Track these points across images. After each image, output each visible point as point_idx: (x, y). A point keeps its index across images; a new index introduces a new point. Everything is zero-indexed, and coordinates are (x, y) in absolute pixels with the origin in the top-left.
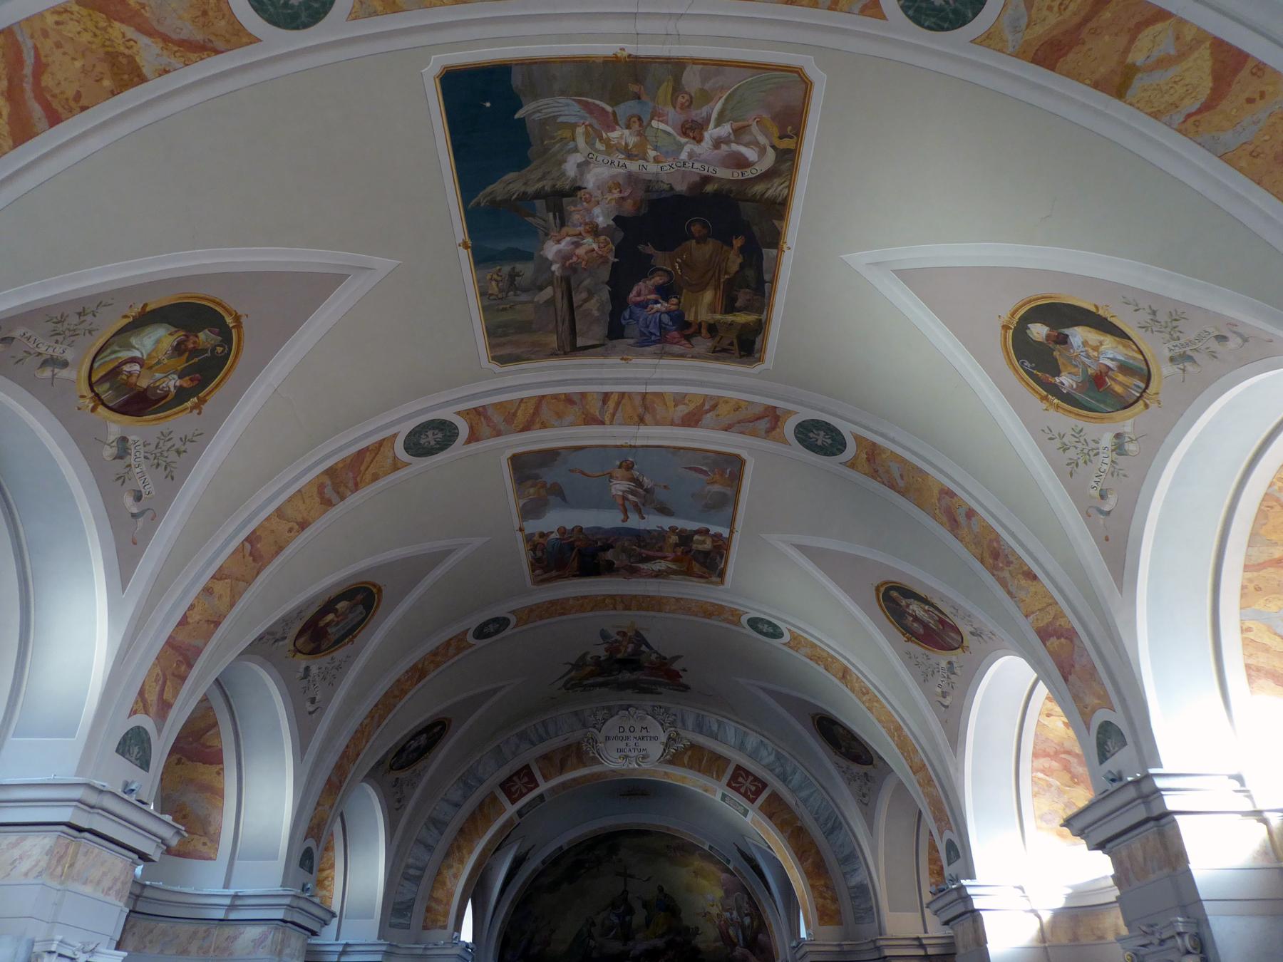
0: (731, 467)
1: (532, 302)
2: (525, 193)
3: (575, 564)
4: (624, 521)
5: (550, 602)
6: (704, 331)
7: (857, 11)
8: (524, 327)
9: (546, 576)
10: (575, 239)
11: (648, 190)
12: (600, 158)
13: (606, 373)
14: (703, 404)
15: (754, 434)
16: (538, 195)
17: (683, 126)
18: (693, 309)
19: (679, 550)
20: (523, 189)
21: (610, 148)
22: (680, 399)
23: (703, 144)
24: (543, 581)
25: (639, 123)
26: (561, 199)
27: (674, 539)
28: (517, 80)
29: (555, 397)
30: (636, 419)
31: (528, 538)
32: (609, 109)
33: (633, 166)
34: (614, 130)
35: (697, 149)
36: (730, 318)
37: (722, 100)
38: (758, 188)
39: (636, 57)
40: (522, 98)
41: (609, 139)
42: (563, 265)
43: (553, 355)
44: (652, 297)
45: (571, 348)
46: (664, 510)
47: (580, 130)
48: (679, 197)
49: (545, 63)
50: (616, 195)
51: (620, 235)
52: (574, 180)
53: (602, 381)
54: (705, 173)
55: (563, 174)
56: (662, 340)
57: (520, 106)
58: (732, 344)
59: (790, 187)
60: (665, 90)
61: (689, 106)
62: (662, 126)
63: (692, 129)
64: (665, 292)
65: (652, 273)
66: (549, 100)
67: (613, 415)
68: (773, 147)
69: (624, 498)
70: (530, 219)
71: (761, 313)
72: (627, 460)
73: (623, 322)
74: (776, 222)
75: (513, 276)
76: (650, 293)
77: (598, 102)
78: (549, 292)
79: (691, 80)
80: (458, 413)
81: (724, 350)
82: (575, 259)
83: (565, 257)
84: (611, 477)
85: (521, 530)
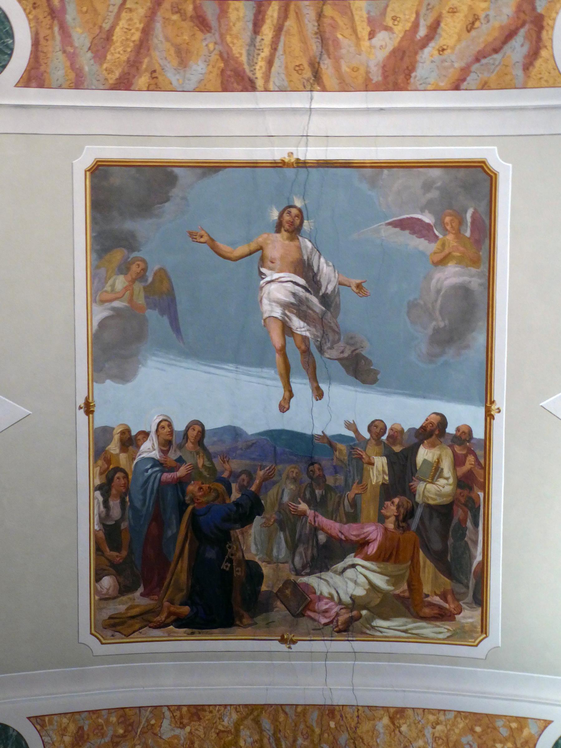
0: (467, 192)
3: (181, 572)
4: (284, 408)
5: (123, 714)
9: (119, 607)
14: (416, 26)
15: (504, 84)
19: (391, 509)
24: (115, 627)
27: (379, 468)
30: (308, 73)
31: (100, 438)
46: (360, 370)
67: (270, 63)
69: (286, 330)
72: (292, 196)
84: (262, 261)
85: (88, 408)
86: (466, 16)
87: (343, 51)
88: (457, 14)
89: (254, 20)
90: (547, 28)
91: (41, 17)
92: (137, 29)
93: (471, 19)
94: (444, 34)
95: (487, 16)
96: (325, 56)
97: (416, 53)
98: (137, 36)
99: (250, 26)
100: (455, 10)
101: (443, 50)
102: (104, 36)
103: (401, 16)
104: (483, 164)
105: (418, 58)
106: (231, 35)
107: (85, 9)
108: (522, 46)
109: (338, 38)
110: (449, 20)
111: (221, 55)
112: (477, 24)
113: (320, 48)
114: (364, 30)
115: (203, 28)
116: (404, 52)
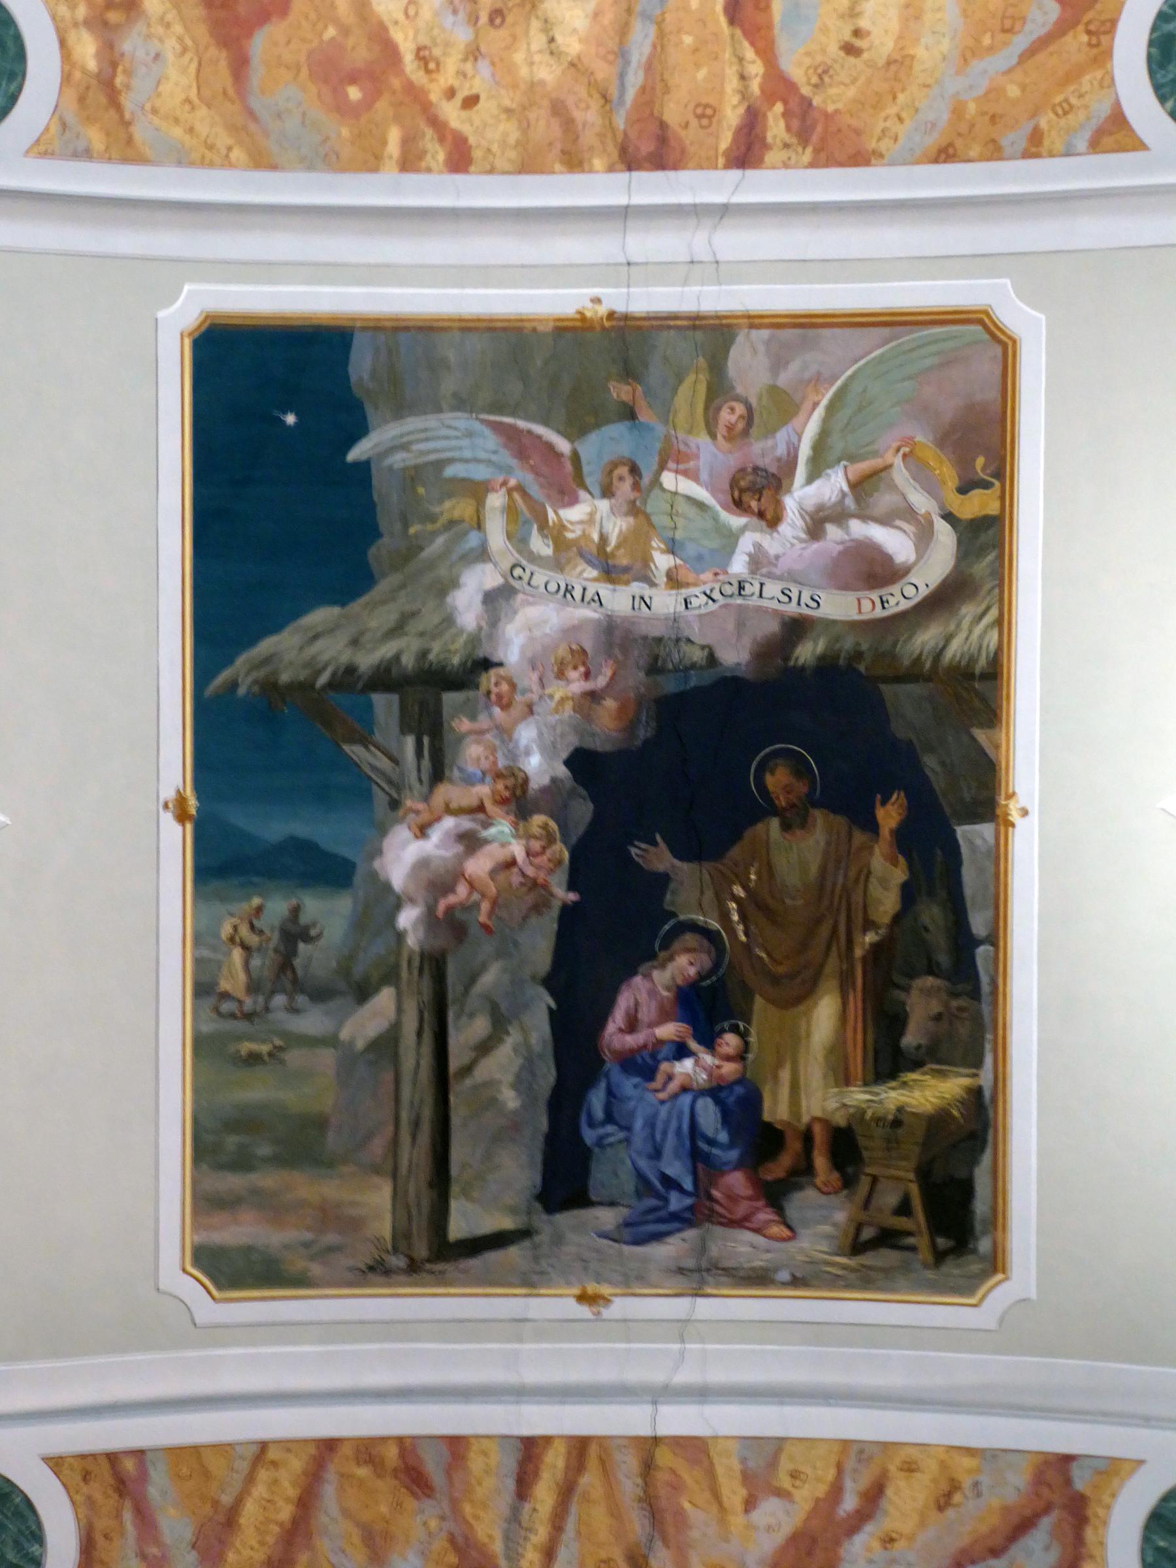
1: (331, 1041)
2: (351, 670)
6: (821, 1161)
7: (1081, 145)
8: (302, 1143)
10: (466, 823)
11: (654, 668)
12: (539, 579)
13: (540, 1364)
14: (836, 1491)
16: (385, 678)
17: (734, 483)
18: (785, 1075)
20: (345, 658)
21: (565, 549)
22: (765, 1464)
23: (783, 528)
25: (632, 479)
26: (439, 688)
28: (362, 365)
29: (367, 1450)
32: (563, 445)
33: (619, 600)
34: (574, 501)
35: (772, 544)
36: (891, 1097)
37: (819, 413)
38: (926, 638)
39: (626, 317)
40: (369, 410)
41: (561, 527)
42: (430, 910)
43: (376, 1272)
44: (668, 1031)
45: (433, 1251)
47: (496, 500)
48: (731, 687)
49: (426, 331)
50: (577, 685)
51: (583, 811)
52: (475, 640)
53: (521, 1393)
54: (792, 609)
55: (449, 620)
56: (700, 1213)
57: (360, 430)
58: (904, 1209)
59: (1003, 623)
60: (691, 393)
61: (746, 432)
62: (687, 486)
63: (758, 492)
64: (707, 1009)
65: (666, 945)
66: (430, 421)
68: (948, 517)
70: (355, 751)
71: (978, 1063)
73: (589, 1136)
74: (980, 735)
75: (295, 933)
76: (664, 1017)
77: (540, 430)
78: (385, 998)
79: (748, 365)
80: (56, 1463)
81: (887, 1238)
82: (462, 890)
83: (438, 882)
86: (934, 1481)
87: (695, 1534)
88: (918, 1475)
89: (518, 1474)
90: (1093, 1520)
91: (98, 1497)
92: (287, 1500)
93: (944, 1486)
94: (891, 1509)
95: (976, 1484)
96: (658, 1544)
97: (838, 1543)
98: (286, 1512)
99: (511, 1484)
100: (914, 1466)
101: (892, 1540)
102: (221, 1518)
103: (809, 1471)
104: (982, 316)
105: (842, 1552)
106: (472, 1501)
107: (185, 1471)
108: (1047, 1548)
109: (683, 1508)
110: (902, 1484)
111: (452, 1540)
112: (957, 1498)
113: (648, 1529)
114: (733, 1493)
115: (415, 1489)
116: (814, 1541)
